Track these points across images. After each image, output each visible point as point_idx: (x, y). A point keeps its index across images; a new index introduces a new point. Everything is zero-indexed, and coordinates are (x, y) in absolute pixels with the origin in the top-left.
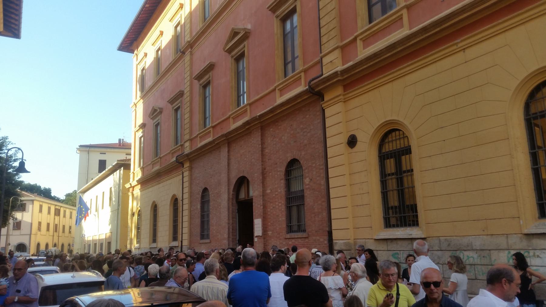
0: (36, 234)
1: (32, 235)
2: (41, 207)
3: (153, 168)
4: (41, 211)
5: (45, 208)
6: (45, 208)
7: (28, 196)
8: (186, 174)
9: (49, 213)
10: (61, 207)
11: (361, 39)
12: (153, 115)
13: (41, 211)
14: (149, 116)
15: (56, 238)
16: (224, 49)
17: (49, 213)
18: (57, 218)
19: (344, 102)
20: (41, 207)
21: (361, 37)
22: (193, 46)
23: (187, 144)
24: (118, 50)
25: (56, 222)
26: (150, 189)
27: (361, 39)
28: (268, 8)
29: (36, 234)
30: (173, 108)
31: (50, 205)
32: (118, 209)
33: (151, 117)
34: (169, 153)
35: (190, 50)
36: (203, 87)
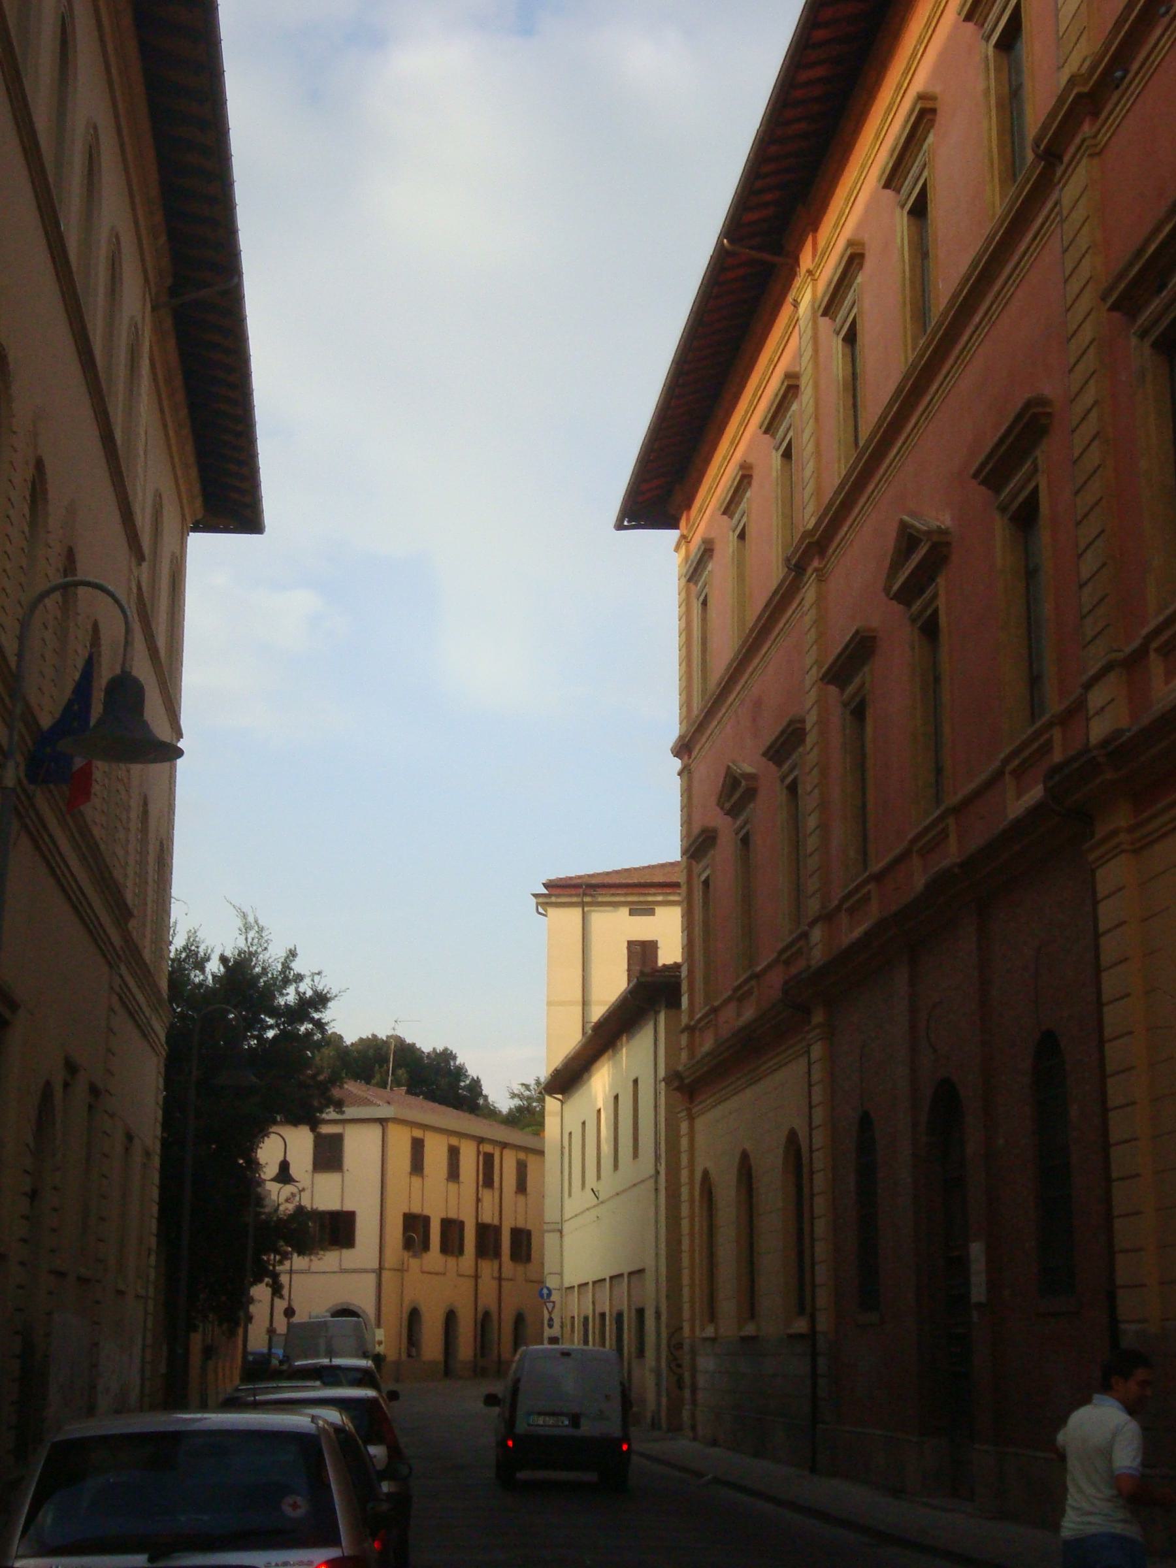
0: (401, 1270)
1: (386, 1275)
2: (418, 1146)
3: (739, 1015)
4: (417, 1166)
5: (436, 1151)
6: (436, 1151)
7: (366, 1102)
8: (817, 1051)
9: (454, 1174)
10: (504, 1145)
11: (1156, 650)
12: (730, 796)
13: (417, 1166)
14: (720, 804)
15: (487, 1284)
16: (887, 590)
17: (454, 1174)
18: (487, 1196)
19: (1136, 852)
20: (418, 1146)
21: (1154, 645)
22: (827, 547)
23: (817, 934)
24: (620, 526)
25: (488, 1217)
26: (749, 1094)
27: (1156, 650)
28: (975, 476)
29: (401, 1270)
30: (783, 779)
31: (454, 1141)
32: (657, 1172)
33: (727, 806)
34: (776, 961)
35: (816, 563)
36: (852, 713)
